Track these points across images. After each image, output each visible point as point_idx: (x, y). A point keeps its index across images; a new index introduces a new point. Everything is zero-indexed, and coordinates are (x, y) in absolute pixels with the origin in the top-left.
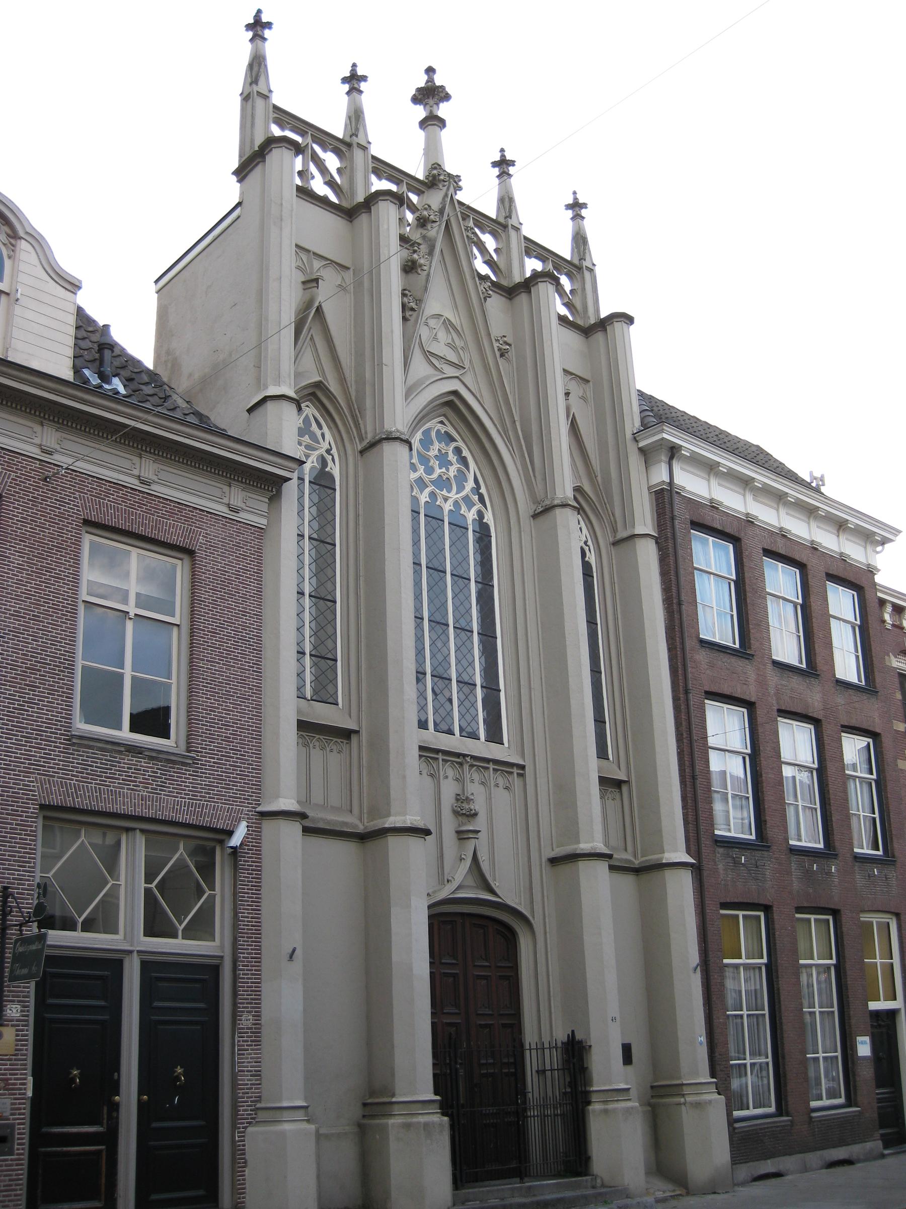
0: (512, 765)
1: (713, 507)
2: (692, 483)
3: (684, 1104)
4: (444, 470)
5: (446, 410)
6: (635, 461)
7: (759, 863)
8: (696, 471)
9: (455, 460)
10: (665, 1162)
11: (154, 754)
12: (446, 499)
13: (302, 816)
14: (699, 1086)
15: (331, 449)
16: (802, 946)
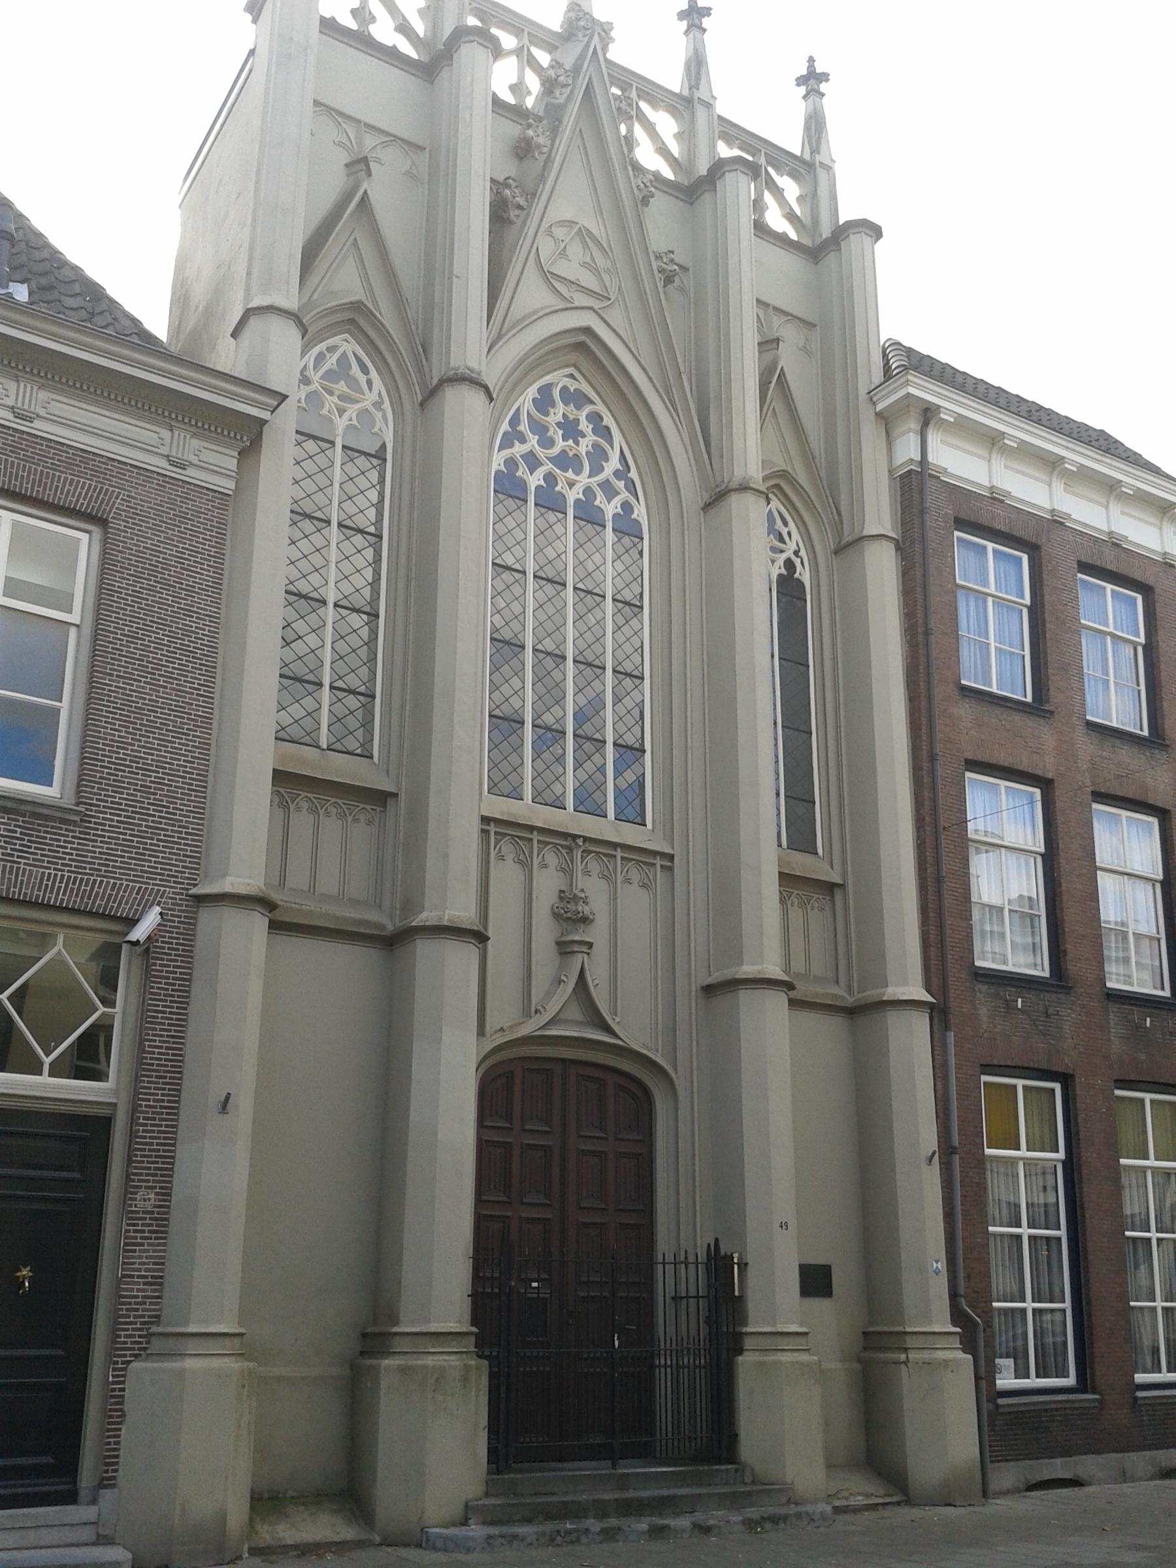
0: (655, 853)
1: (994, 499)
2: (959, 463)
3: (906, 1363)
4: (571, 442)
5: (574, 357)
6: (870, 436)
7: (1051, 1011)
8: (967, 447)
9: (590, 430)
10: (874, 1445)
11: (10, 804)
12: (571, 484)
13: (789, 986)
14: (930, 1338)
15: (382, 402)
16: (1127, 1136)
